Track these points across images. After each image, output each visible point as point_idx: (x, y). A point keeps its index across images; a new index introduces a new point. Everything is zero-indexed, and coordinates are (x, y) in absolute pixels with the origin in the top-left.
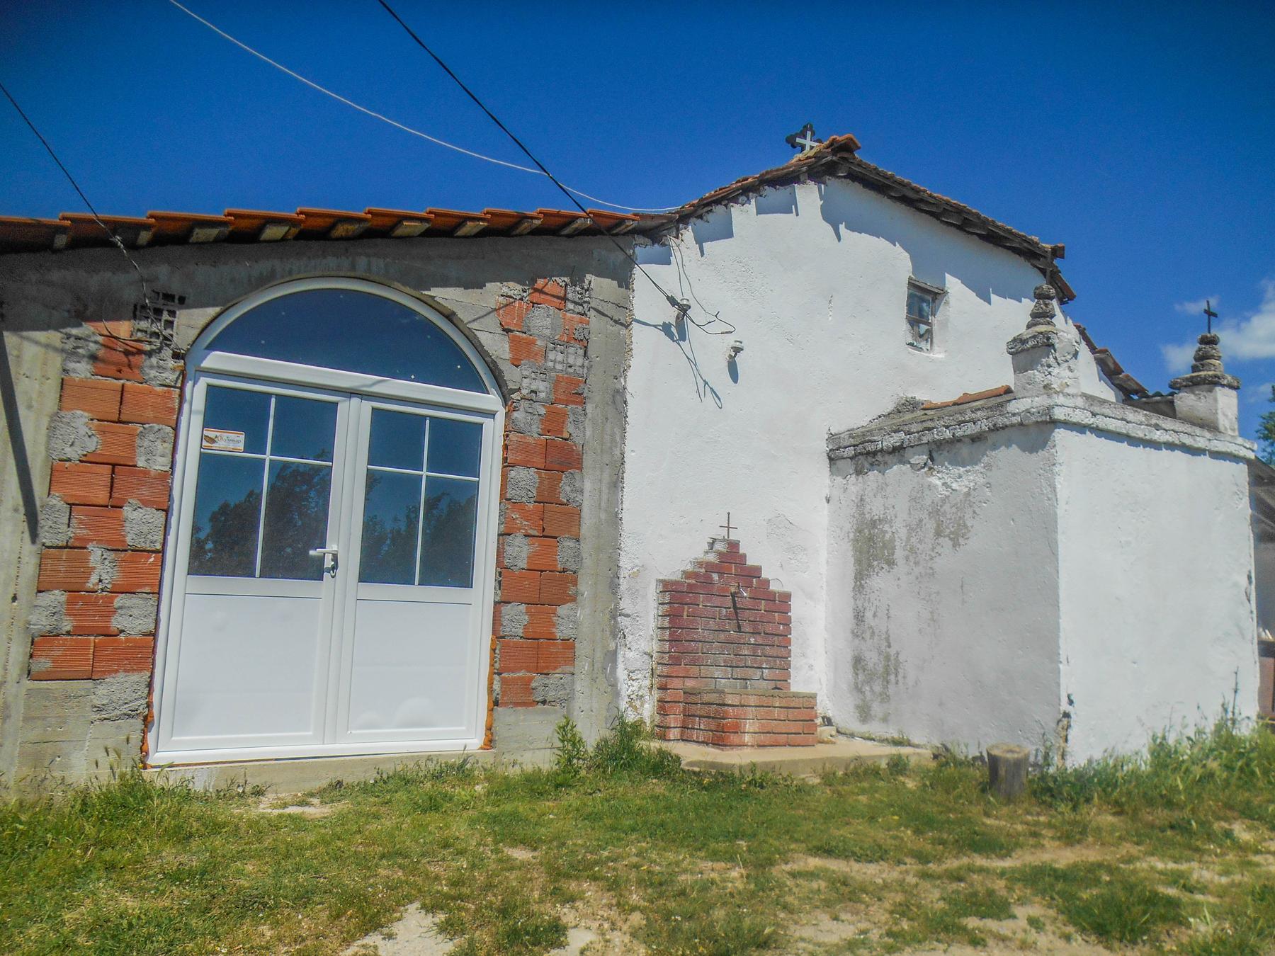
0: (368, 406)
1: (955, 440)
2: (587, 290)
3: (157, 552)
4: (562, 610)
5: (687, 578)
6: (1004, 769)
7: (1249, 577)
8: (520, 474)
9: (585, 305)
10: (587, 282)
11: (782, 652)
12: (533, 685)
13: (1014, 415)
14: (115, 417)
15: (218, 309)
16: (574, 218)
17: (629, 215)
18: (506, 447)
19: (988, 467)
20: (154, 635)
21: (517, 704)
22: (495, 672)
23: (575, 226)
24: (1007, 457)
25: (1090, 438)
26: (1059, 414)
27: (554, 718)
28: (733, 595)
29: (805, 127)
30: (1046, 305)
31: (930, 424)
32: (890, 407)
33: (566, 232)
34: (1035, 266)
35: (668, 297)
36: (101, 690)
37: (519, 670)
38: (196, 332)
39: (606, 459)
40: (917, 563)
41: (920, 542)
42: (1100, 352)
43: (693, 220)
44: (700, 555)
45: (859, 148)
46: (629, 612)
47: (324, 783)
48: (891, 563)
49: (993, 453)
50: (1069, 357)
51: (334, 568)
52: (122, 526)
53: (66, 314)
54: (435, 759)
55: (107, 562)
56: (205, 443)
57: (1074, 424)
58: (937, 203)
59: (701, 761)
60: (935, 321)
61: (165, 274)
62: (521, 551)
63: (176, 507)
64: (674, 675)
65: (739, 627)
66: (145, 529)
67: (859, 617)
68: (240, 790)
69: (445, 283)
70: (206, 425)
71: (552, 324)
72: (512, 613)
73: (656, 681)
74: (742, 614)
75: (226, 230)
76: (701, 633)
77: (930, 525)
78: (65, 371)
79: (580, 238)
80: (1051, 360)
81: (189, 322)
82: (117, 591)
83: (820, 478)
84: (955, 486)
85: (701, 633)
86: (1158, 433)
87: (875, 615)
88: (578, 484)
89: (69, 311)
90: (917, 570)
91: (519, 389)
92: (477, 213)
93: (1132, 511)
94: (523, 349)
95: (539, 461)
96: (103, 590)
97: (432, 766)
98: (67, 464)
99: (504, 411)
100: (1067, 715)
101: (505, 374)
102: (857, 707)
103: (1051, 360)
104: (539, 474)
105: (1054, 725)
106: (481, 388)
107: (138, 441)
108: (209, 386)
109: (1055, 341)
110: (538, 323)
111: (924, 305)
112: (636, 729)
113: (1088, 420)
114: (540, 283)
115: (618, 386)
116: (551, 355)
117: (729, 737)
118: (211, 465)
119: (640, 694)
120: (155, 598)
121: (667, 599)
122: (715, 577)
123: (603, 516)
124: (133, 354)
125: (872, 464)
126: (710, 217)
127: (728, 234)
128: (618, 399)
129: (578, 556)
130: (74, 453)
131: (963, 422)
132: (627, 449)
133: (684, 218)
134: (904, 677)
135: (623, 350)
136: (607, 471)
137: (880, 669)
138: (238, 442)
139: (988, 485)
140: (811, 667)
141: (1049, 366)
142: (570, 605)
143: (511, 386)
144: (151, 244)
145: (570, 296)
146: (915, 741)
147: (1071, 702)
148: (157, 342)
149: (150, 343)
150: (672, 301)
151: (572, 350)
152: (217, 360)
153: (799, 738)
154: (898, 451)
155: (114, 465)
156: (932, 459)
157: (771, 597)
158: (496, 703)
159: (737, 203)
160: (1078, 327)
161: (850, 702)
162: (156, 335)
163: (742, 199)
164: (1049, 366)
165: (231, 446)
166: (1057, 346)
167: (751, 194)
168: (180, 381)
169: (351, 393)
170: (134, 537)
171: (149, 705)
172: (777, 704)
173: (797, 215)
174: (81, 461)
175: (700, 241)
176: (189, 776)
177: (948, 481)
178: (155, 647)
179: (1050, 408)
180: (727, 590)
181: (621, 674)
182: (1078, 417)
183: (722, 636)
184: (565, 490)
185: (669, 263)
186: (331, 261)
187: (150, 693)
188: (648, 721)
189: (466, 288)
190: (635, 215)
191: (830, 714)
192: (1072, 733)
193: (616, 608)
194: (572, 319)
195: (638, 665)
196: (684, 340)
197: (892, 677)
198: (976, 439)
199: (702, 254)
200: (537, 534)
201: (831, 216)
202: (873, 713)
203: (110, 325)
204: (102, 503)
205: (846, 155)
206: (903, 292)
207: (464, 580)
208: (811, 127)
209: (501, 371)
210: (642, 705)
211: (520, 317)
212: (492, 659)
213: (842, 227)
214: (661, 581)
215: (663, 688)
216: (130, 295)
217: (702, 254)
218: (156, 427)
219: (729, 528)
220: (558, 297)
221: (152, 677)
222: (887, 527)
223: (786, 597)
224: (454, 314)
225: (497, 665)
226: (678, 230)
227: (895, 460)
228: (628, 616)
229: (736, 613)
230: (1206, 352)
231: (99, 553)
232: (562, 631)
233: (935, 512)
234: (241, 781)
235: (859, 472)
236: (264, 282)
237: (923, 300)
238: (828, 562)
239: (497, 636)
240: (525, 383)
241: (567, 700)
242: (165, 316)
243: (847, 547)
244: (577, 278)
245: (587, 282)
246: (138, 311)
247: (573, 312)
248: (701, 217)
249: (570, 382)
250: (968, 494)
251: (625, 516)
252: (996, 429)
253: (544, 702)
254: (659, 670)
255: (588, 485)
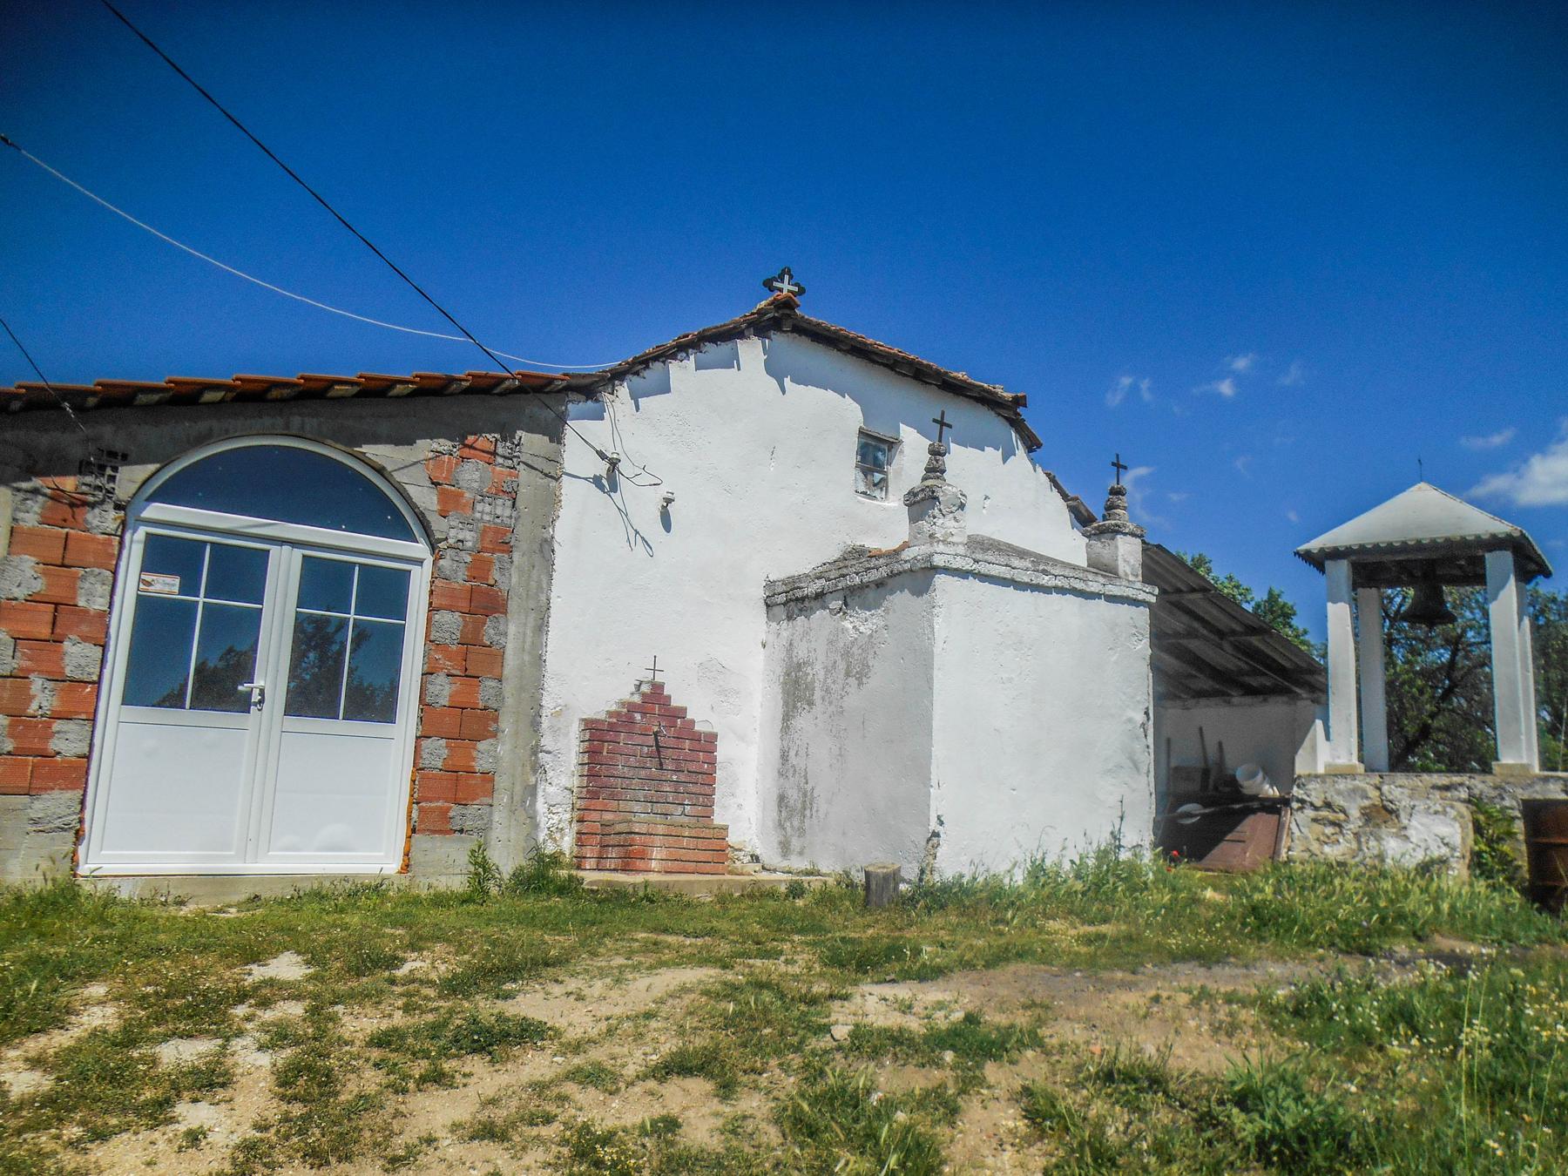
0: (298, 554)
1: (863, 587)
2: (518, 445)
3: (93, 683)
4: (481, 746)
5: (610, 717)
6: (874, 883)
7: (1147, 713)
8: (444, 617)
9: (515, 460)
10: (517, 438)
11: (707, 790)
12: (451, 814)
13: (906, 562)
14: (59, 563)
15: (158, 466)
16: (503, 380)
17: (558, 375)
18: (431, 592)
19: (887, 611)
20: (88, 757)
21: (435, 832)
22: (414, 801)
23: (504, 386)
24: (901, 600)
25: (973, 583)
26: (939, 561)
27: (471, 842)
28: (656, 734)
29: (783, 270)
30: (937, 461)
31: (845, 571)
32: (837, 555)
33: (497, 391)
34: (999, 414)
35: (597, 452)
36: (38, 805)
37: (438, 799)
38: (137, 486)
39: (532, 604)
40: (830, 703)
41: (834, 682)
42: (1072, 499)
43: (629, 376)
44: (626, 697)
45: (798, 306)
46: (550, 749)
47: (243, 897)
48: (811, 703)
49: (891, 598)
50: (955, 508)
51: (261, 702)
52: (62, 659)
53: (17, 470)
54: (351, 879)
55: (46, 691)
56: (142, 586)
57: (956, 570)
58: (888, 356)
59: (600, 881)
60: (891, 470)
61: (109, 433)
62: (443, 690)
63: (112, 643)
64: (592, 808)
65: (661, 764)
66: (83, 662)
67: (784, 757)
68: (163, 899)
69: (376, 439)
70: (144, 569)
71: (481, 477)
72: (432, 747)
73: (576, 814)
74: (664, 753)
75: (167, 395)
76: (620, 770)
77: (842, 665)
78: (15, 519)
79: (511, 396)
80: (936, 511)
81: (129, 478)
82: (57, 716)
83: (756, 624)
84: (862, 629)
85: (620, 770)
86: (1047, 578)
87: (796, 755)
88: (501, 628)
89: (20, 467)
90: (832, 709)
91: (446, 539)
92: (408, 377)
93: (1015, 650)
94: (450, 501)
95: (464, 605)
96: (42, 716)
97: (348, 886)
98: (14, 602)
99: (432, 559)
100: (936, 834)
101: (433, 524)
102: (780, 843)
103: (936, 511)
104: (464, 618)
105: (924, 843)
106: (408, 536)
107: (79, 584)
108: (147, 534)
109: (939, 494)
110: (467, 477)
111: (880, 454)
112: (555, 860)
113: (967, 564)
114: (471, 439)
115: (545, 536)
116: (479, 507)
117: (635, 863)
118: (147, 607)
119: (560, 826)
120: (89, 724)
121: (587, 737)
122: (638, 717)
123: (527, 658)
124: (78, 506)
125: (801, 610)
126: (646, 373)
127: (665, 389)
128: (546, 548)
129: (499, 695)
130: (21, 593)
131: (869, 569)
132: (553, 595)
133: (618, 375)
134: (817, 811)
135: (551, 503)
136: (533, 615)
137: (799, 806)
138: (173, 585)
139: (886, 627)
140: (740, 806)
141: (934, 517)
142: (491, 741)
143: (438, 536)
144: (98, 407)
145: (500, 451)
146: (824, 871)
147: (941, 823)
148: (100, 495)
149: (94, 495)
150: (602, 455)
151: (500, 502)
152: (156, 511)
153: (708, 867)
154: (820, 596)
155: (56, 604)
156: (846, 604)
157: (696, 737)
158: (414, 831)
159: (676, 359)
160: (1048, 475)
161: (774, 838)
162: (99, 488)
163: (682, 355)
164: (934, 517)
165: (167, 589)
166: (941, 499)
167: (690, 351)
168: (120, 530)
169: (281, 542)
170: (73, 669)
171: (81, 821)
172: (687, 834)
173: (739, 369)
174: (26, 600)
175: (635, 397)
176: (115, 885)
177: (857, 624)
178: (88, 768)
179: (931, 555)
180: (650, 729)
181: (541, 807)
182: (958, 563)
183: (643, 773)
184: (489, 632)
185: (602, 419)
186: (267, 421)
187: (82, 810)
188: (567, 853)
189: (396, 445)
190: (564, 375)
191: (758, 852)
192: (940, 852)
193: (537, 745)
194: (501, 473)
195: (559, 799)
196: (615, 492)
197: (808, 813)
198: (879, 584)
199: (638, 409)
200: (458, 673)
201: (775, 370)
202: (792, 847)
203: (58, 480)
204: (43, 637)
205: (787, 311)
206: (853, 443)
207: (386, 713)
208: (789, 271)
209: (429, 522)
210: (562, 838)
211: (449, 471)
212: (412, 789)
213: (787, 381)
214: (583, 720)
215: (581, 821)
216: (77, 452)
217: (638, 409)
218: (97, 570)
219: (654, 670)
220: (488, 452)
221: (84, 795)
222: (809, 670)
223: (712, 738)
224: (384, 468)
225: (416, 795)
226: (614, 386)
227: (818, 606)
228: (549, 752)
229: (659, 752)
230: (1112, 503)
231: (40, 683)
232: (481, 764)
233: (847, 654)
234: (164, 892)
235: (790, 618)
236: (202, 440)
237: (880, 450)
238: (762, 706)
239: (417, 768)
240: (452, 533)
241: (485, 830)
242: (109, 472)
243: (778, 689)
244: (507, 433)
245: (517, 438)
246: (83, 468)
247: (503, 465)
248: (637, 373)
249: (497, 531)
250: (871, 636)
251: (549, 657)
252: (892, 575)
253: (461, 831)
254: (579, 804)
255: (512, 629)
